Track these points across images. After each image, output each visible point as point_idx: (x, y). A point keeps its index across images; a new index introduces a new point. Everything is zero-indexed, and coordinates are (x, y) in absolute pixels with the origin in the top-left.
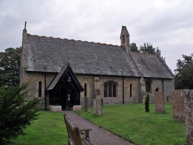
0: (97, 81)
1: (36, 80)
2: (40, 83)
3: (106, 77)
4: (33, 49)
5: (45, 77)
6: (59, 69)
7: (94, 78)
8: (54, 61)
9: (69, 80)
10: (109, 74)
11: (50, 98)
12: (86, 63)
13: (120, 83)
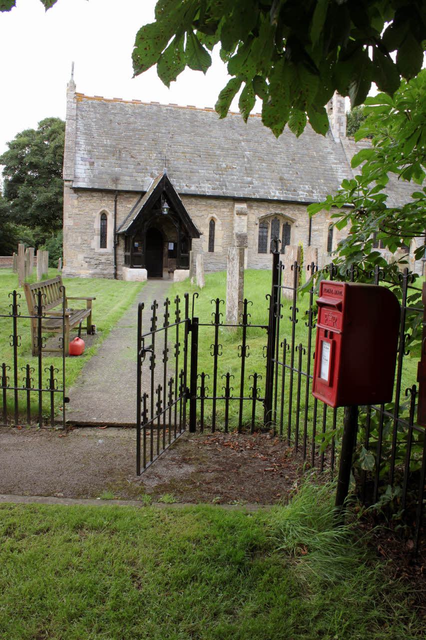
0: (240, 213)
1: (98, 206)
2: (104, 217)
3: (266, 204)
4: (89, 135)
5: (116, 201)
6: (149, 185)
7: (234, 206)
8: (139, 164)
9: (165, 210)
10: (274, 196)
11: (126, 249)
12: (218, 167)
13: (301, 218)
